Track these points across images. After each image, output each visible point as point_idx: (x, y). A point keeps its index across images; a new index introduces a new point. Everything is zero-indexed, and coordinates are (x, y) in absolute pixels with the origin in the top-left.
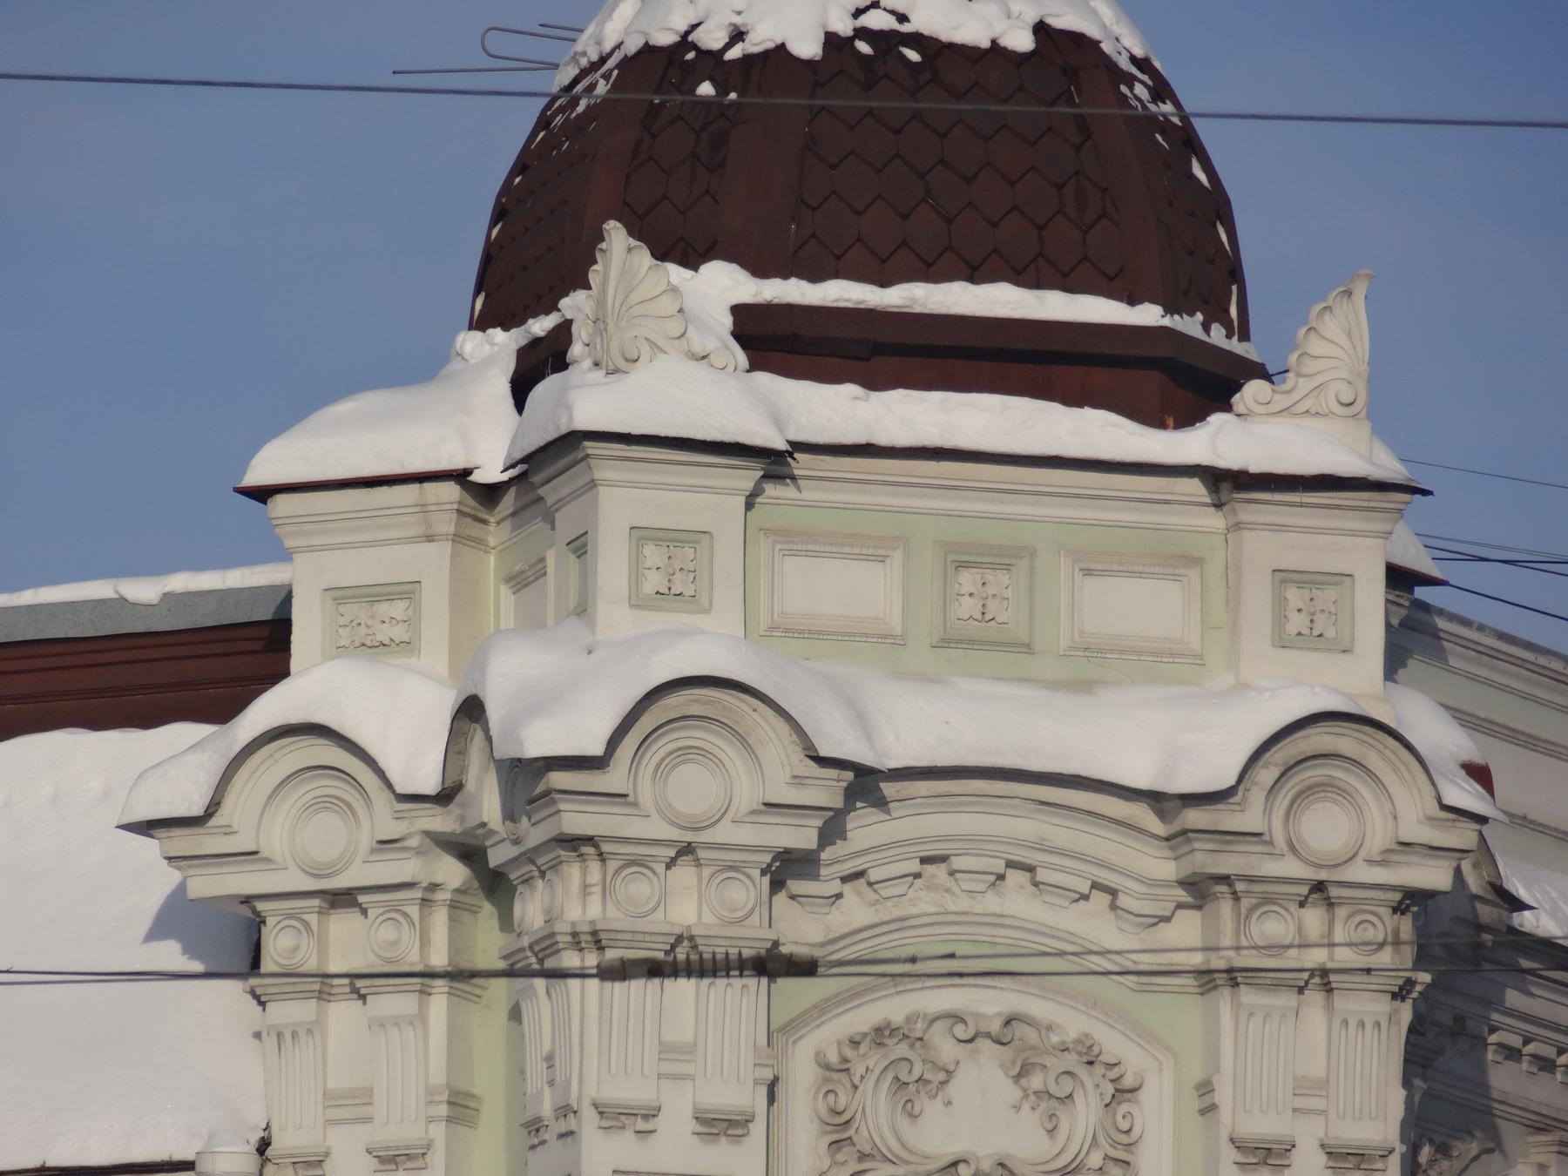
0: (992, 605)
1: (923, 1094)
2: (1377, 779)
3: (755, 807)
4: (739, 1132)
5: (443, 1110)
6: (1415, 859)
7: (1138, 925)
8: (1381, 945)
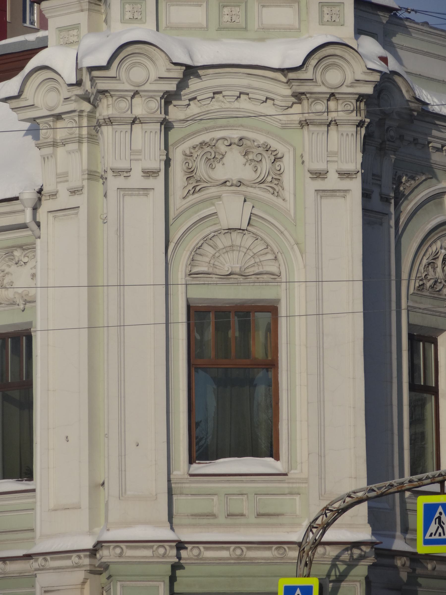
0: (234, 18)
1: (215, 162)
2: (345, 59)
3: (156, 79)
4: (156, 175)
5: (86, 176)
6: (361, 85)
7: (281, 109)
8: (352, 111)
